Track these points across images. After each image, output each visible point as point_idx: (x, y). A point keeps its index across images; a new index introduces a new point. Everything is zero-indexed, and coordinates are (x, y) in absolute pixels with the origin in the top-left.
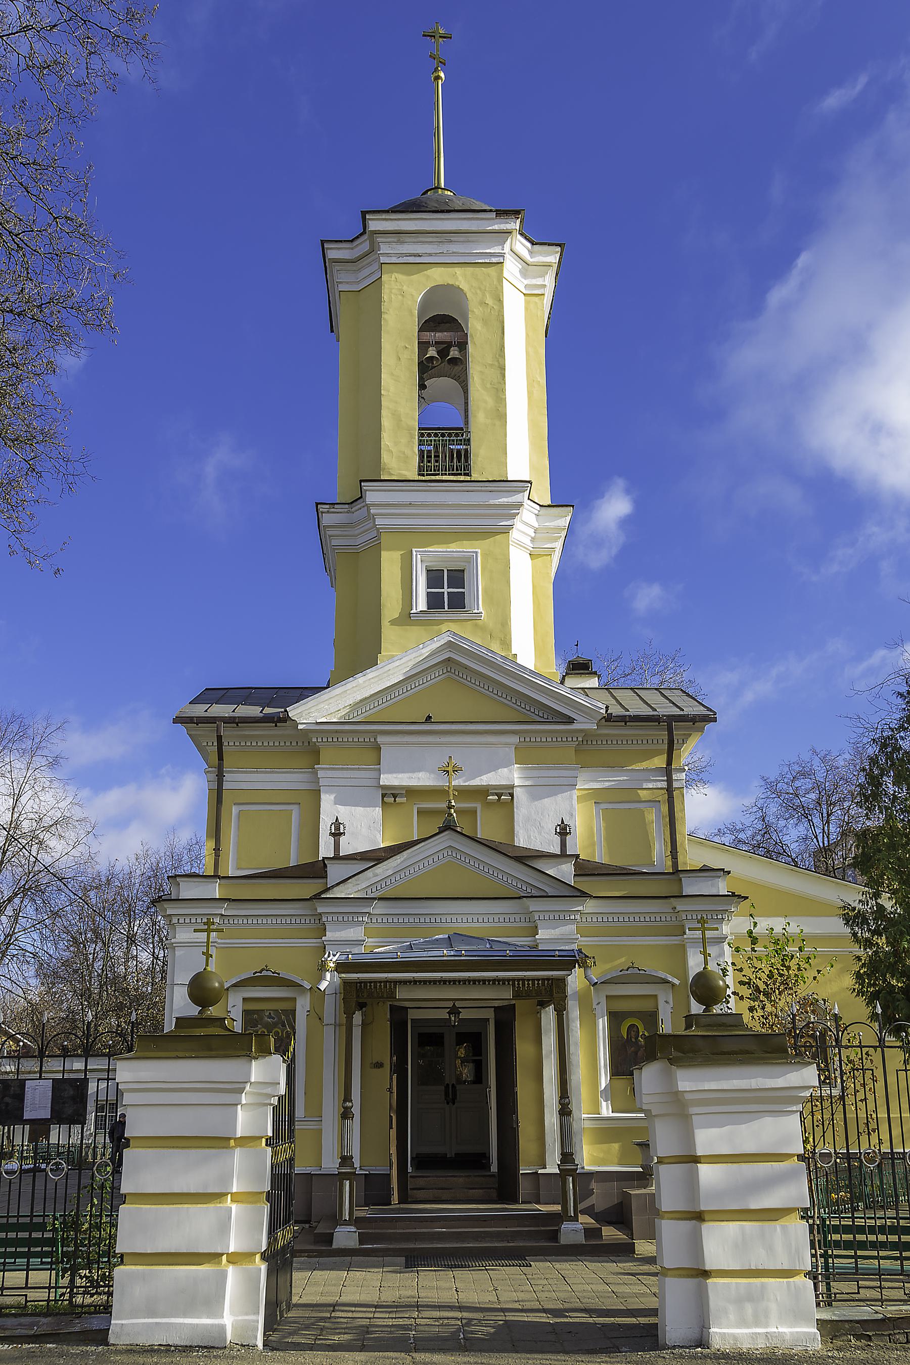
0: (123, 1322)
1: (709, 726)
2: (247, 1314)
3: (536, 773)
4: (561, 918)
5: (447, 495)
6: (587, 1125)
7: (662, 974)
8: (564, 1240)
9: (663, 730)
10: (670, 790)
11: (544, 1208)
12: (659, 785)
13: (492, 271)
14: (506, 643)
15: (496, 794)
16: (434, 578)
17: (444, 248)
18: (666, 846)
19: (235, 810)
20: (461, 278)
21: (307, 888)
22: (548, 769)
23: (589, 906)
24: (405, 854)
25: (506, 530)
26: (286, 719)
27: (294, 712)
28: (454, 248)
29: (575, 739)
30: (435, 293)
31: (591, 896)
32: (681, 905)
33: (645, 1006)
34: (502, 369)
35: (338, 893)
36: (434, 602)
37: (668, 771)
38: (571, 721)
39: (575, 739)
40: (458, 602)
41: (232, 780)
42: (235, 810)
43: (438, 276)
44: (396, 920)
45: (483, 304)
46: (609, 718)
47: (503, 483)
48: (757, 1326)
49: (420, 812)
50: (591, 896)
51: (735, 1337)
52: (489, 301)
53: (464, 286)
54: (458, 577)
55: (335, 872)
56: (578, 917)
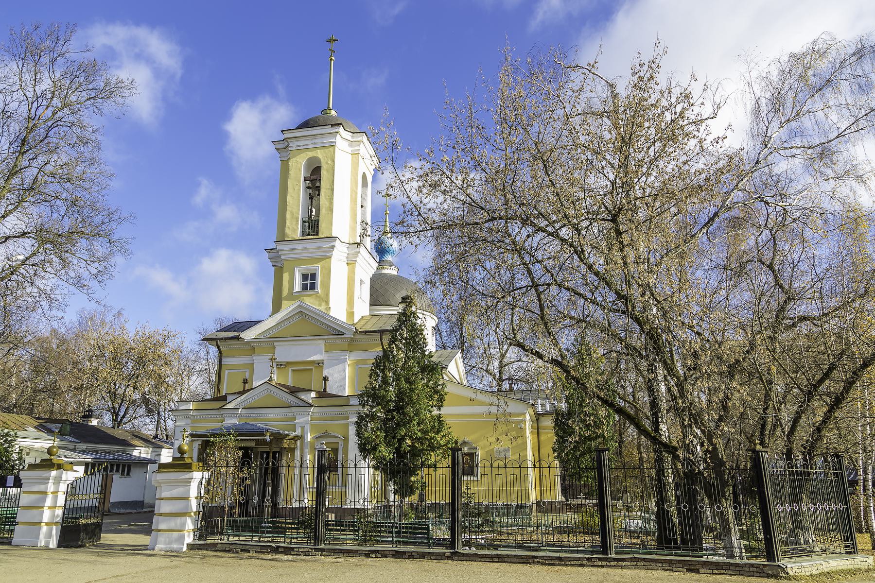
4: (304, 414)
5: (311, 246)
7: (337, 435)
11: (678, 365)
13: (331, 149)
14: (325, 299)
16: (305, 277)
17: (313, 141)
19: (227, 372)
20: (319, 154)
21: (218, 404)
25: (330, 257)
26: (238, 338)
27: (242, 335)
28: (317, 141)
30: (310, 161)
32: (347, 408)
34: (333, 190)
35: (228, 406)
36: (305, 287)
40: (313, 286)
41: (225, 361)
42: (227, 372)
43: (311, 154)
45: (327, 163)
47: (332, 238)
49: (293, 370)
52: (330, 162)
53: (320, 156)
54: (313, 276)
55: (229, 398)
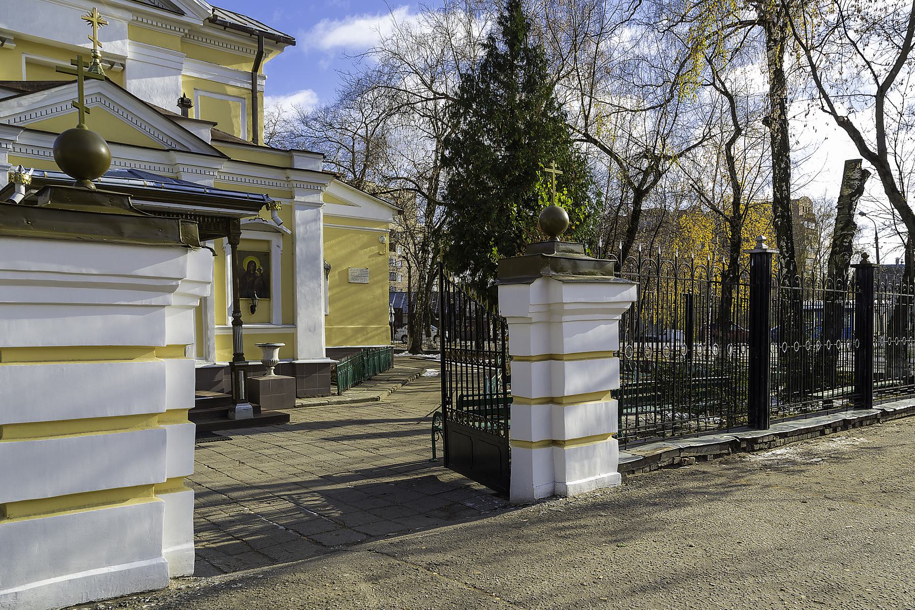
0: (17, 589)
1: (289, 48)
2: (178, 544)
3: (146, 51)
6: (217, 332)
8: (238, 417)
9: (254, 42)
10: (254, 91)
12: (246, 86)
15: (109, 62)
18: (249, 134)
22: (158, 50)
23: (225, 166)
24: (46, 93)
29: (182, 30)
31: (229, 159)
32: (293, 176)
33: (262, 248)
37: (253, 77)
38: (182, 13)
39: (182, 30)
44: (35, 152)
46: (213, 20)
48: (589, 476)
50: (229, 159)
51: (580, 486)
56: (216, 174)
